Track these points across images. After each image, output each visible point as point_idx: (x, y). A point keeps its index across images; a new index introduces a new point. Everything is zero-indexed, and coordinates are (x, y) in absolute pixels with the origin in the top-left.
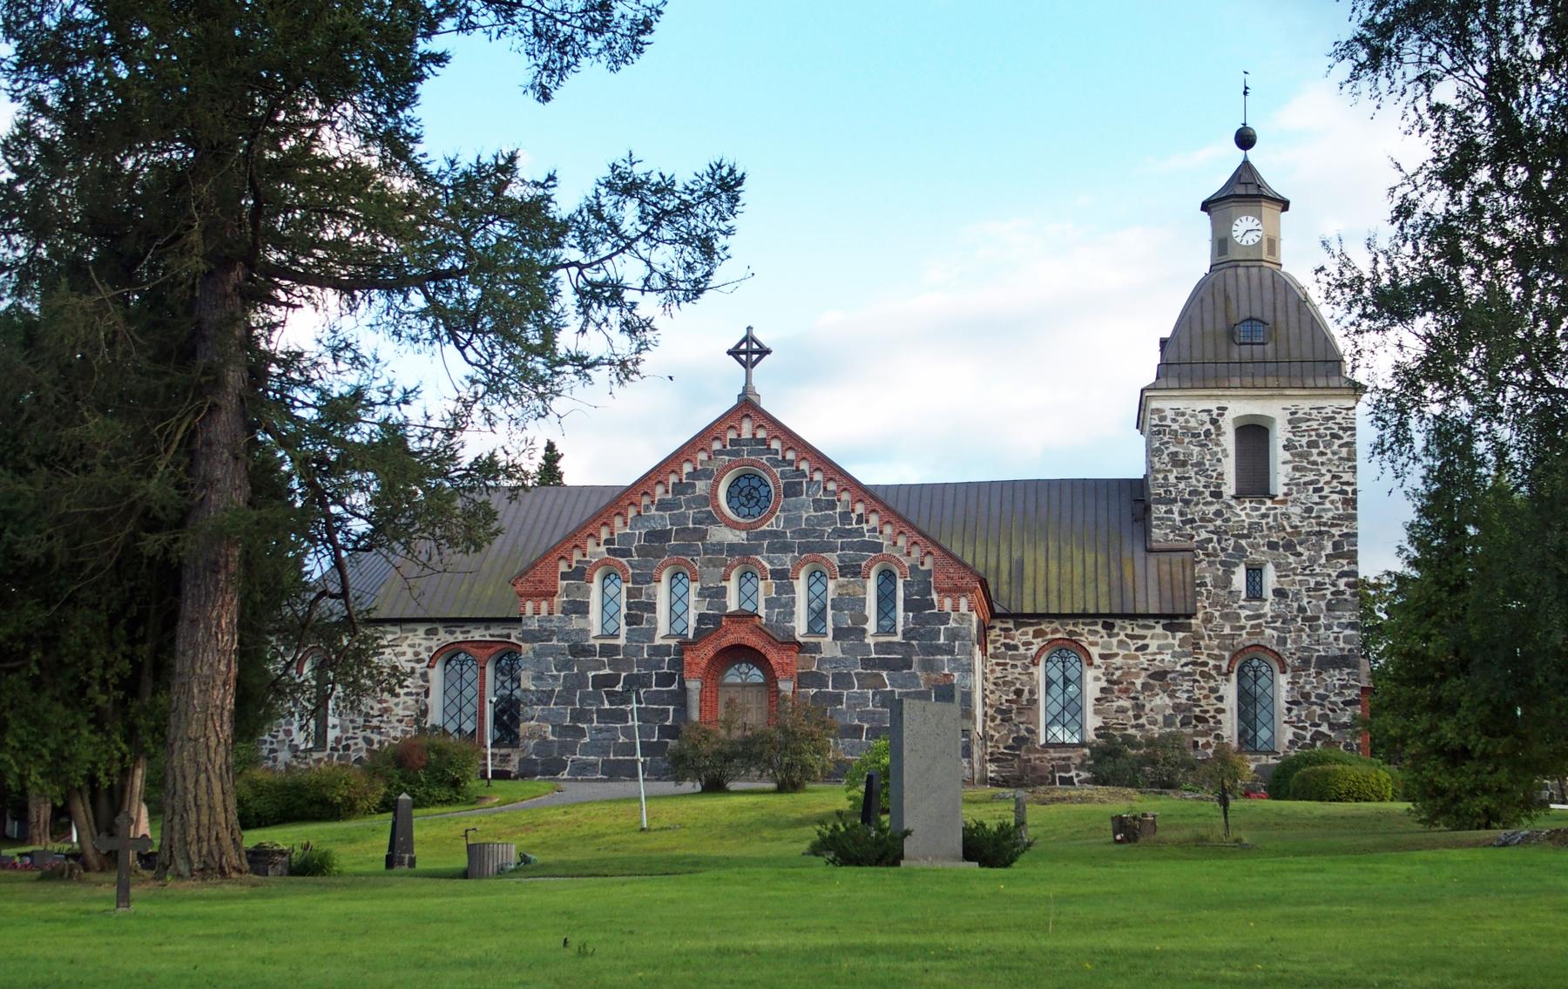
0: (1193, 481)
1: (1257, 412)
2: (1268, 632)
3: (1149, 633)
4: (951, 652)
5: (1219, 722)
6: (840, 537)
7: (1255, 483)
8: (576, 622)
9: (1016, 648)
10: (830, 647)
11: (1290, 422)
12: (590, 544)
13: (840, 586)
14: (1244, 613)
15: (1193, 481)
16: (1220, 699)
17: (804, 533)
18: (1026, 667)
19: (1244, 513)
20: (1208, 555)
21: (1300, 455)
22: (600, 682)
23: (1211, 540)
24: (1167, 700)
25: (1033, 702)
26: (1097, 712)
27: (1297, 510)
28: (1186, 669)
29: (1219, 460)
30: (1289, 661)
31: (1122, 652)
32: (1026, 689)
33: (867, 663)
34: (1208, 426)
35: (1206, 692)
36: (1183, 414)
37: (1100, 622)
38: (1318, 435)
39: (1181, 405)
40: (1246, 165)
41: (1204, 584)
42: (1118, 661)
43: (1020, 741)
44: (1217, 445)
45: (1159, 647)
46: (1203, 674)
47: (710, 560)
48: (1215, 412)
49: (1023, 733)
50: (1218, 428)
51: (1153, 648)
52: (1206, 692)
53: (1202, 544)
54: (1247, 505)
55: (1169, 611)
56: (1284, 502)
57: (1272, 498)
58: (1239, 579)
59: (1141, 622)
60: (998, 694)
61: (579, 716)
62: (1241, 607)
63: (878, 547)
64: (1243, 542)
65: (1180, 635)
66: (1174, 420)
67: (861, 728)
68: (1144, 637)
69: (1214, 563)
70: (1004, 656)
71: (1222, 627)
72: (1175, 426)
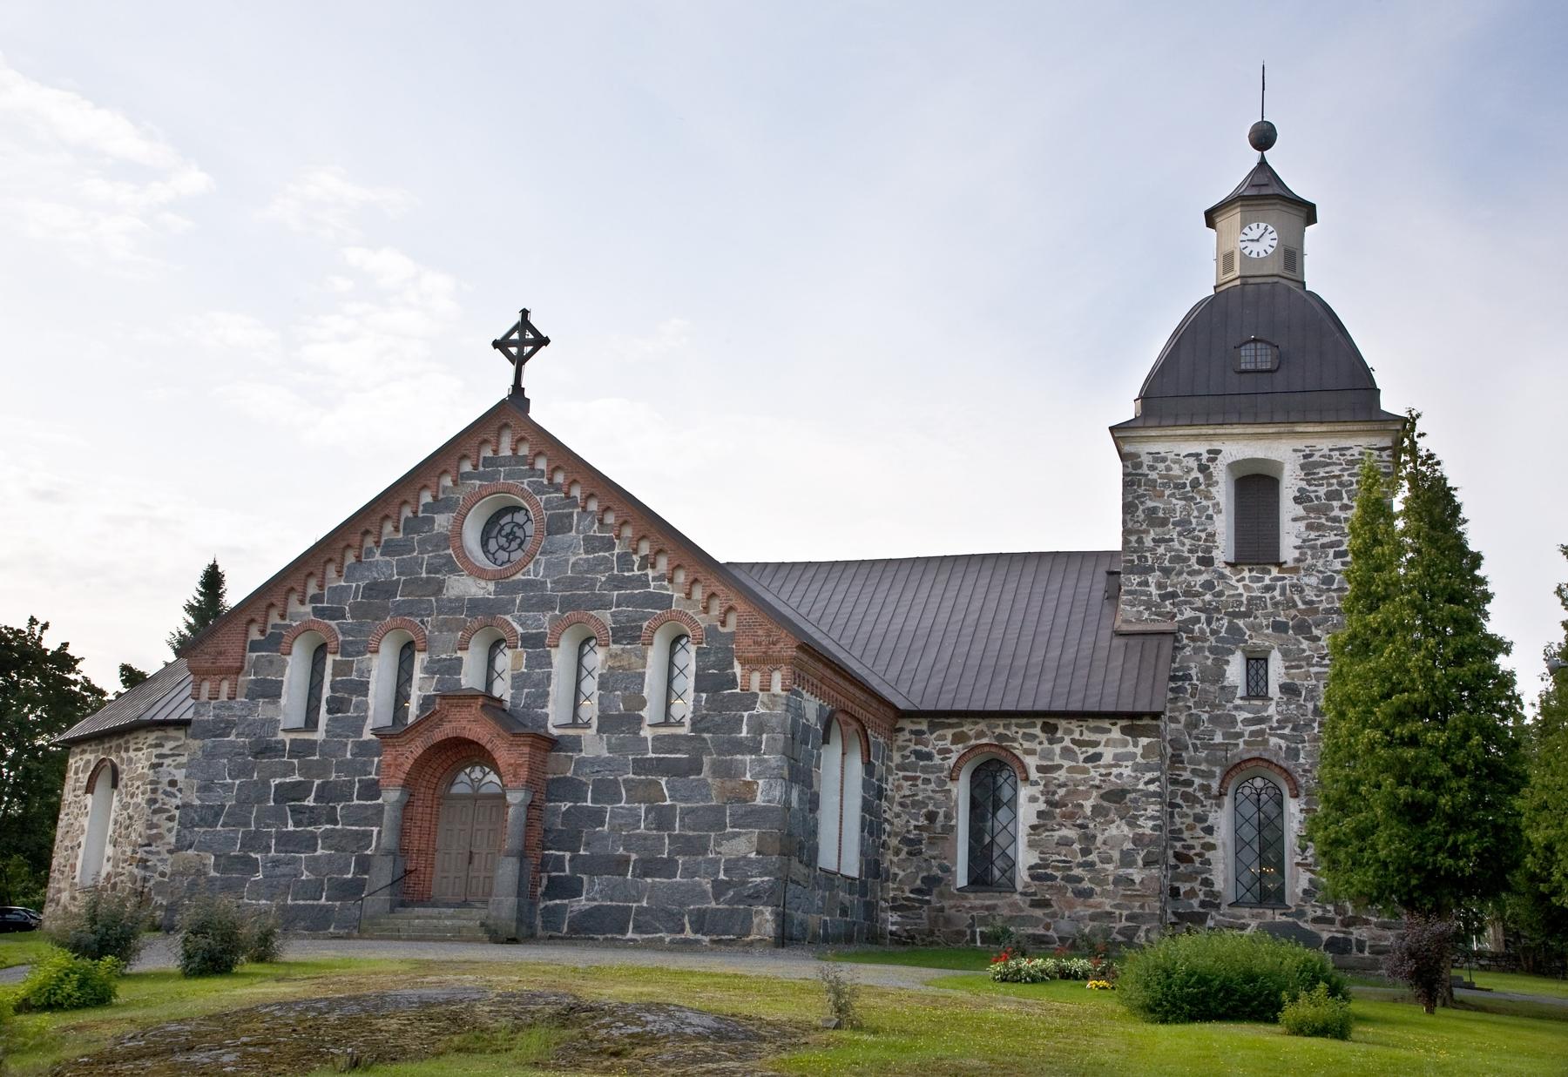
0: (1176, 545)
1: (1260, 455)
2: (1273, 741)
3: (1103, 738)
4: (756, 750)
5: (1208, 862)
6: (618, 588)
7: (1257, 546)
8: (263, 710)
9: (929, 756)
10: (594, 745)
11: (1303, 467)
12: (294, 606)
13: (613, 656)
14: (1242, 716)
15: (1176, 545)
16: (1209, 830)
17: (572, 583)
18: (941, 783)
19: (1243, 584)
20: (1193, 639)
21: (1317, 510)
22: (288, 794)
23: (1198, 620)
24: (1126, 829)
25: (950, 829)
26: (1032, 845)
27: (1314, 581)
28: (1152, 788)
29: (1210, 517)
30: (1302, 781)
31: (1067, 764)
32: (942, 812)
33: (641, 766)
34: (1195, 474)
35: (1189, 821)
36: (1164, 460)
37: (1039, 723)
38: (1341, 484)
39: (1160, 447)
40: (1263, 163)
41: (1188, 677)
42: (1062, 775)
43: (931, 882)
44: (1207, 498)
45: (1116, 757)
46: (1185, 796)
47: (445, 622)
48: (1205, 456)
49: (936, 871)
50: (1209, 476)
51: (1108, 757)
52: (1189, 821)
53: (1186, 626)
54: (1246, 574)
55: (1128, 708)
56: (1295, 570)
57: (1279, 565)
58: (1235, 671)
59: (1092, 723)
60: (905, 817)
61: (254, 841)
62: (1237, 708)
63: (665, 602)
64: (1241, 623)
65: (1144, 741)
66: (1152, 468)
67: (627, 860)
68: (1096, 744)
69: (1201, 649)
70: (913, 767)
71: (1212, 734)
72: (1153, 475)
